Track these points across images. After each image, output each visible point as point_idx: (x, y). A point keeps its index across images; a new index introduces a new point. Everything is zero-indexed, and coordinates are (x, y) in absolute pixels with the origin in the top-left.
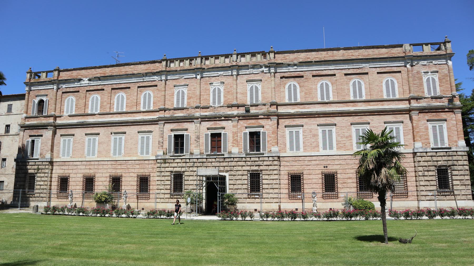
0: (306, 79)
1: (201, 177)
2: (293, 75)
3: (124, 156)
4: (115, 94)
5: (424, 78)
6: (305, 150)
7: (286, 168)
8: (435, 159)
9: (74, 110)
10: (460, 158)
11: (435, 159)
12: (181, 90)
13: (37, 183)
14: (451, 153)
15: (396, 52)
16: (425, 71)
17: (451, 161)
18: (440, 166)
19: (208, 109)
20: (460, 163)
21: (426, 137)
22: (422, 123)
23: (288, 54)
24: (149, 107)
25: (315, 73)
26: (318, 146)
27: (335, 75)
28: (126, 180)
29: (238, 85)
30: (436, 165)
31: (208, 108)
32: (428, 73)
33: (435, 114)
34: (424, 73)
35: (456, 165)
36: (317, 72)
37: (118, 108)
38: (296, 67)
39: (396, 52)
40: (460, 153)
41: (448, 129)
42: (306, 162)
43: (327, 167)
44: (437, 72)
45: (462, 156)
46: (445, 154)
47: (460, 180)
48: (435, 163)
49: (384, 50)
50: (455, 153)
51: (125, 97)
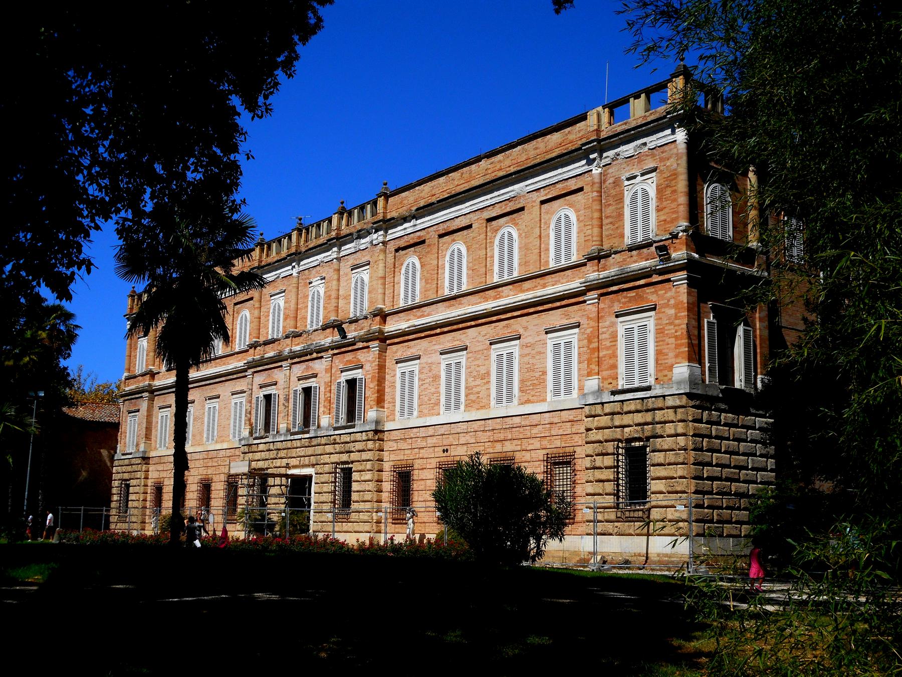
0: (429, 246)
1: (284, 479)
2: (412, 242)
3: (421, 414)
4: (551, 213)
5: (626, 193)
6: (421, 414)
7: (393, 457)
8: (618, 421)
9: (464, 279)
10: (670, 415)
11: (618, 421)
12: (638, 188)
13: (652, 472)
14: (650, 404)
15: (576, 135)
16: (628, 175)
17: (610, 428)
18: (629, 441)
19: (302, 338)
20: (669, 429)
21: (611, 362)
22: (607, 323)
23: (569, 129)
24: (568, 255)
25: (442, 229)
26: (437, 403)
27: (469, 227)
28: (421, 477)
29: (342, 279)
30: (619, 437)
31: (300, 335)
32: (635, 177)
33: (632, 294)
34: (628, 179)
35: (662, 437)
36: (445, 226)
37: (558, 258)
38: (413, 222)
39: (576, 135)
40: (670, 402)
41: (659, 332)
42: (419, 440)
43: (447, 451)
44: (654, 170)
45: (675, 408)
46: (639, 407)
47: (666, 478)
48: (618, 433)
49: (556, 137)
50: (660, 403)
51: (515, 235)
